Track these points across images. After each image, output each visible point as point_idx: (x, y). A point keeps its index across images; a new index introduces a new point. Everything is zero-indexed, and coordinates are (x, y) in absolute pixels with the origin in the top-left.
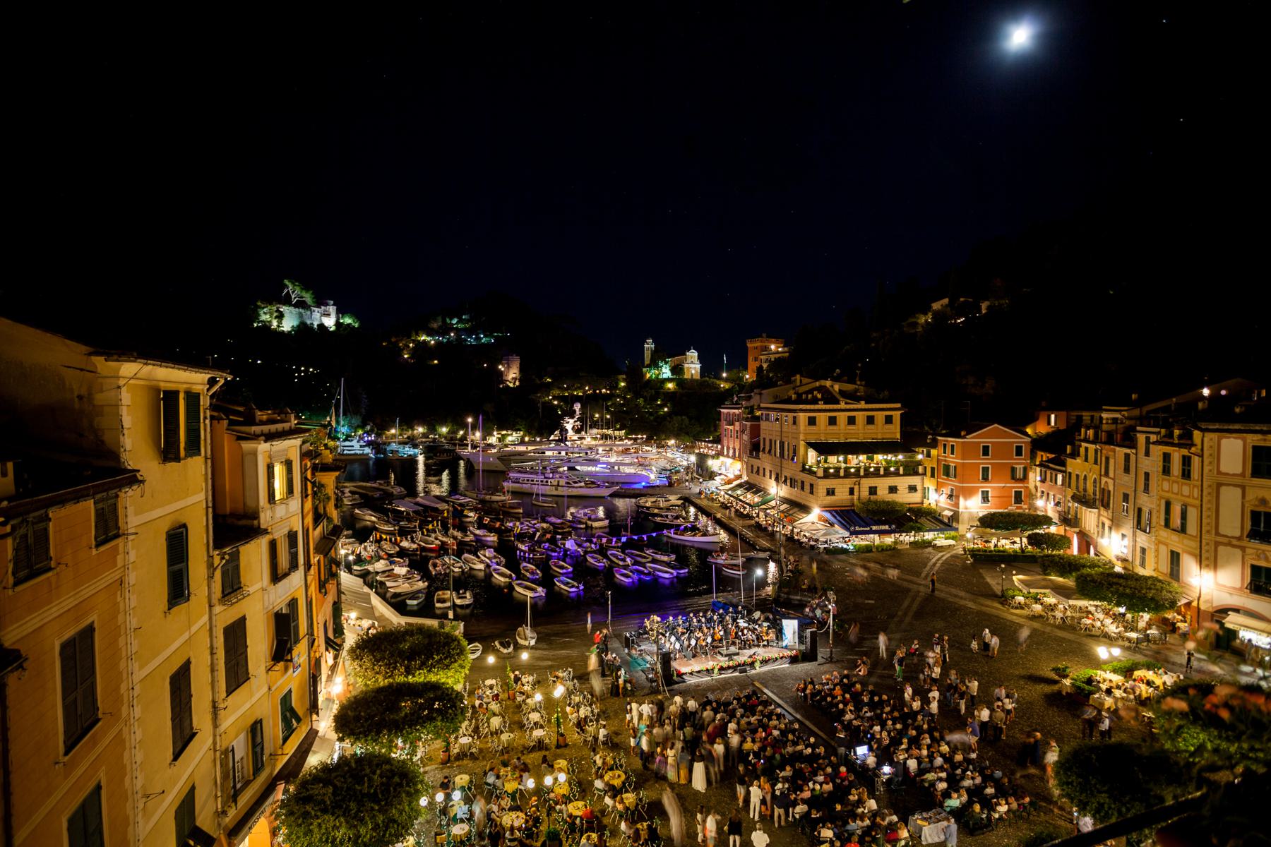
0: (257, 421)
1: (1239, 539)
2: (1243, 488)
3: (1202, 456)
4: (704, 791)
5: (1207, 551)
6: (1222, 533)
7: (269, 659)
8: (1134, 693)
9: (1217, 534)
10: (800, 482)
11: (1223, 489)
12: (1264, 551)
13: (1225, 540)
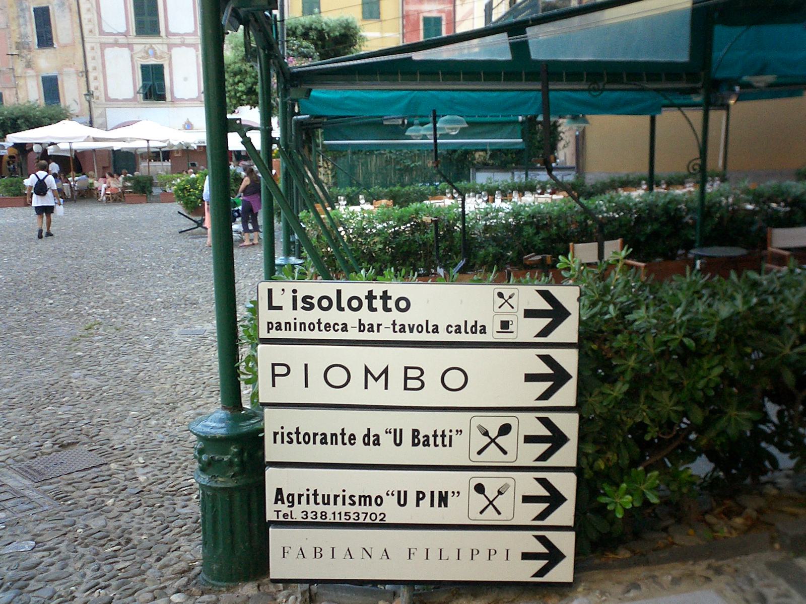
1: (126, 34)
5: (94, 58)
8: (595, 412)
9: (102, 33)
12: (151, 44)
13: (111, 39)
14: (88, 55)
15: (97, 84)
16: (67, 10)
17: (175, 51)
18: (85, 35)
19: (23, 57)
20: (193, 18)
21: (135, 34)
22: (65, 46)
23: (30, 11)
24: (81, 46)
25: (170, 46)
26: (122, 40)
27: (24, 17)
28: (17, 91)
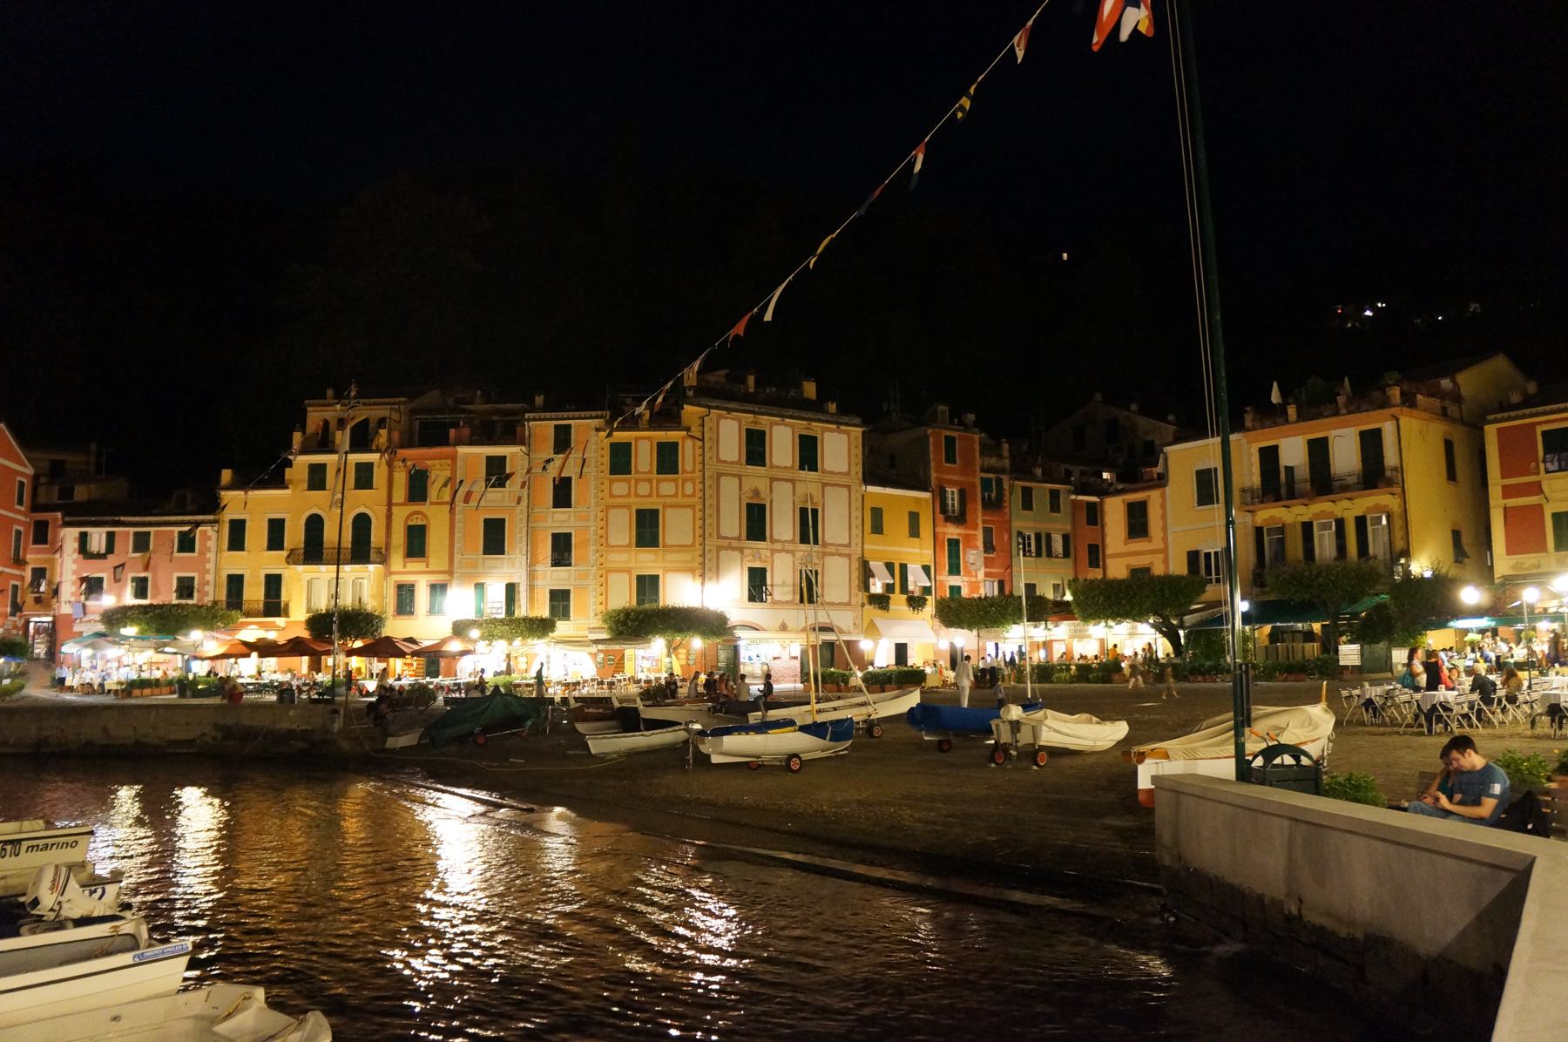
2: (740, 477)
3: (702, 440)
9: (719, 537)
10: (217, 517)
11: (723, 480)
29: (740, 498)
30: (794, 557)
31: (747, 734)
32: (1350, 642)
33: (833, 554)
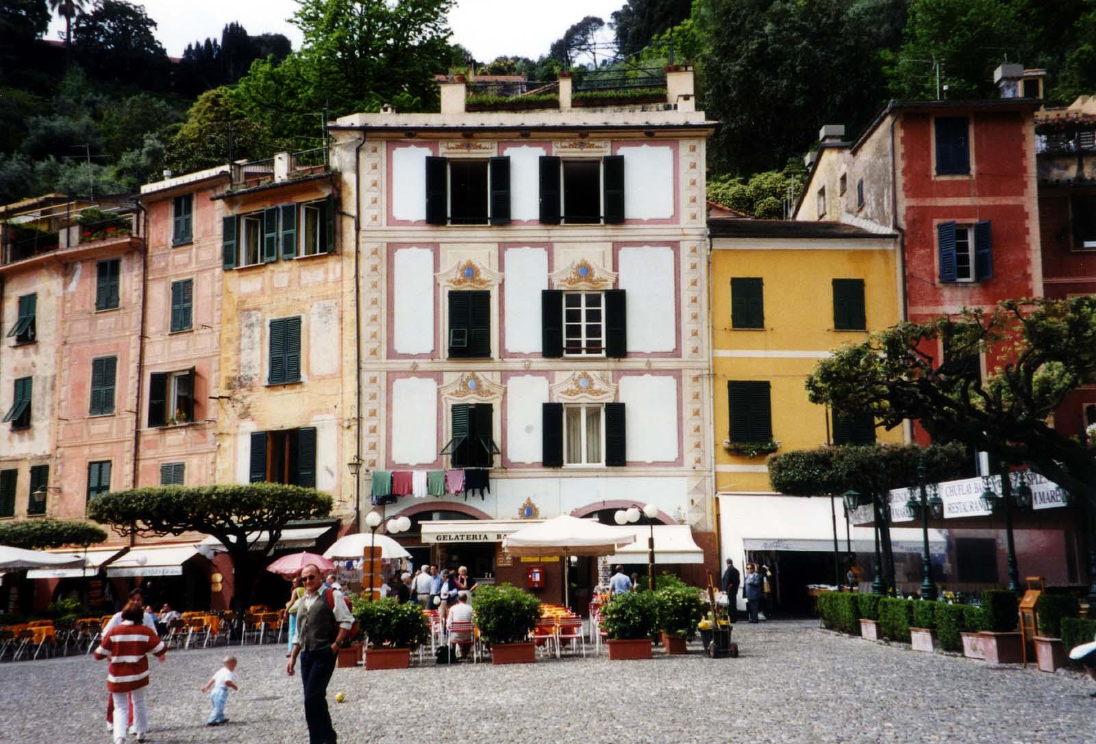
0: (596, 515)
4: (175, 52)
6: (336, 363)
7: (625, 226)
9: (391, 354)
11: (401, 255)
13: (406, 364)
14: (364, 390)
15: (374, 457)
16: (334, 322)
17: (513, 382)
18: (363, 359)
19: (237, 401)
20: (539, 480)
21: (447, 355)
22: (322, 378)
23: (263, 327)
24: (361, 273)
25: (506, 375)
26: (424, 365)
27: (250, 337)
28: (215, 457)
29: (436, 285)
30: (551, 381)
31: (43, 549)
32: (989, 496)
33: (639, 372)
